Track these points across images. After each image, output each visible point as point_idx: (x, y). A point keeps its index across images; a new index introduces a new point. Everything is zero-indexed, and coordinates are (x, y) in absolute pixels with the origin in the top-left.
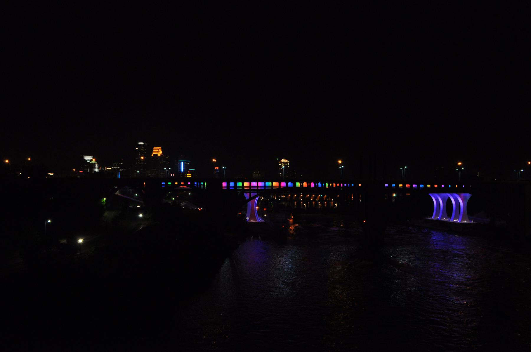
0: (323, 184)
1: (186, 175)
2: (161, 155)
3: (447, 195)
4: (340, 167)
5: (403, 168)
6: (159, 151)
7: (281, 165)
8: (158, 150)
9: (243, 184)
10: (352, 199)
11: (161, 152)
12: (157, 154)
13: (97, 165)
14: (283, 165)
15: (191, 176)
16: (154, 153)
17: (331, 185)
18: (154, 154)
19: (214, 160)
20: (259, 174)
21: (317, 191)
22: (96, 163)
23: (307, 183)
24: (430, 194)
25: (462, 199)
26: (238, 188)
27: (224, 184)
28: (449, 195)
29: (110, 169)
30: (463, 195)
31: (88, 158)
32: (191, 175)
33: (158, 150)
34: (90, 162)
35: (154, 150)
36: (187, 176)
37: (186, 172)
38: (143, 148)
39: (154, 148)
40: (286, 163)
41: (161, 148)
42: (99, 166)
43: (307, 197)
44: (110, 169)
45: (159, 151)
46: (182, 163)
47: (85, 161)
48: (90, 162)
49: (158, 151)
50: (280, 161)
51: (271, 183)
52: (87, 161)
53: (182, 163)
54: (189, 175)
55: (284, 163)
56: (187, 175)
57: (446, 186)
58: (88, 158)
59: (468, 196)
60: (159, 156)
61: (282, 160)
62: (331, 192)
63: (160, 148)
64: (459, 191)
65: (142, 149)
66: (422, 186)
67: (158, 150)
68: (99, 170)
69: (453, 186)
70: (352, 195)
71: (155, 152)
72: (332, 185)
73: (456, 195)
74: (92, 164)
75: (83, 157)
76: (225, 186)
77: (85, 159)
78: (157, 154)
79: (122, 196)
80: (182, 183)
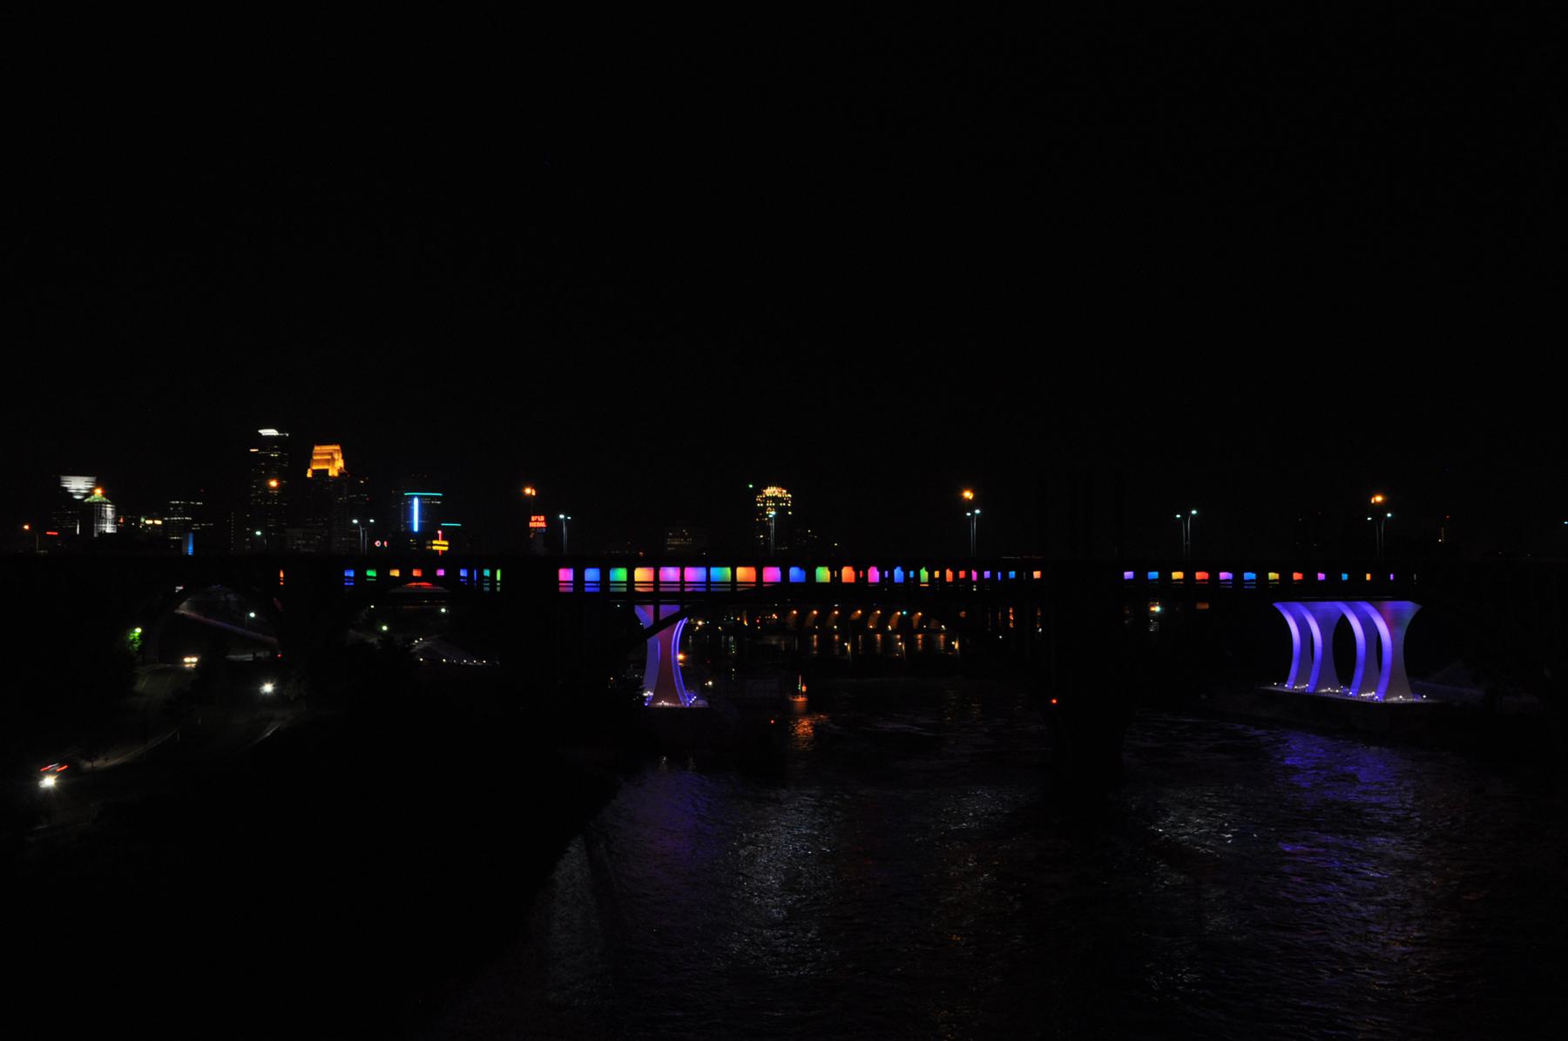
0: (937, 574)
1: (429, 542)
2: (341, 474)
3: (1339, 610)
4: (969, 514)
5: (1186, 514)
6: (333, 460)
7: (765, 508)
8: (329, 457)
9: (631, 575)
10: (1011, 625)
11: (340, 463)
12: (327, 471)
13: (109, 511)
14: (772, 507)
15: (446, 548)
16: (315, 467)
17: (937, 574)
18: (314, 471)
19: (528, 491)
21: (888, 595)
22: (107, 503)
23: (830, 570)
24: (1278, 606)
25: (1384, 620)
26: (612, 590)
27: (566, 575)
28: (1342, 607)
29: (159, 522)
30: (1389, 605)
31: (77, 485)
32: (446, 543)
33: (329, 457)
34: (86, 500)
35: (315, 458)
36: (434, 548)
37: (428, 533)
38: (276, 450)
39: (317, 449)
40: (782, 500)
41: (341, 448)
42: (117, 513)
43: (854, 617)
44: (159, 522)
45: (332, 461)
46: (416, 501)
47: (68, 495)
48: (86, 500)
49: (330, 461)
50: (761, 493)
51: (728, 571)
52: (72, 494)
53: (416, 501)
54: (440, 545)
55: (775, 499)
56: (435, 542)
57: (1357, 577)
58: (77, 485)
59: (1409, 609)
60: (333, 477)
61: (766, 488)
62: (937, 600)
63: (338, 447)
64: (1374, 594)
65: (273, 450)
66: (1249, 576)
67: (331, 454)
68: (118, 528)
69: (1357, 577)
70: (1011, 611)
71: (319, 462)
72: (943, 575)
73: (1368, 608)
74: (92, 504)
75: (59, 482)
76: (728, 583)
77: (66, 488)
78: (327, 471)
79: (202, 618)
80: (416, 573)
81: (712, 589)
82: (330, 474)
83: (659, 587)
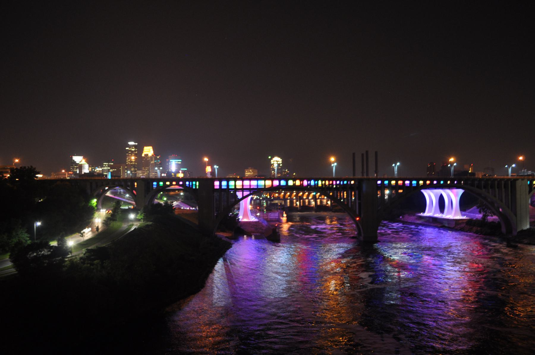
17: (349, 182)
20: (251, 172)
57: (445, 182)
67: (149, 149)
81: (259, 187)
82: (149, 155)
83: (229, 187)
